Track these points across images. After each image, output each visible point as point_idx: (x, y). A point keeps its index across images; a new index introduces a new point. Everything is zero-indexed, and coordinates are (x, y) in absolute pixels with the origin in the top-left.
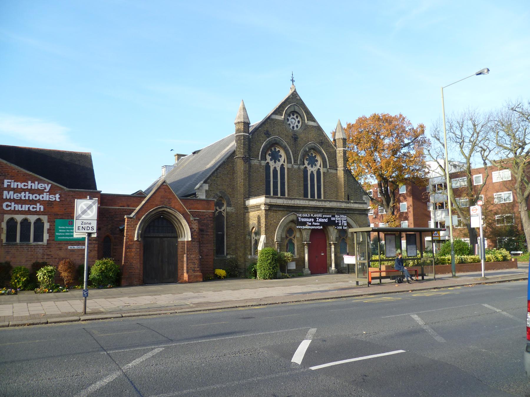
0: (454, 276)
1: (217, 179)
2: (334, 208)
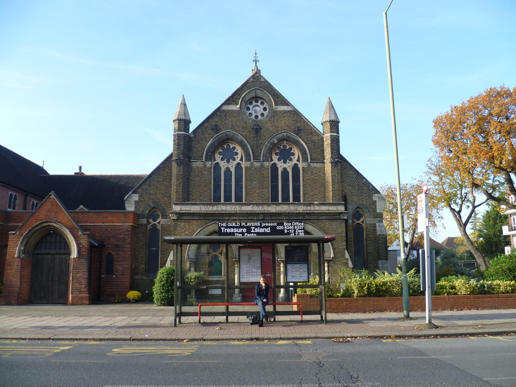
0: (408, 317)
1: (149, 187)
2: (283, 213)
